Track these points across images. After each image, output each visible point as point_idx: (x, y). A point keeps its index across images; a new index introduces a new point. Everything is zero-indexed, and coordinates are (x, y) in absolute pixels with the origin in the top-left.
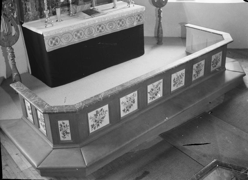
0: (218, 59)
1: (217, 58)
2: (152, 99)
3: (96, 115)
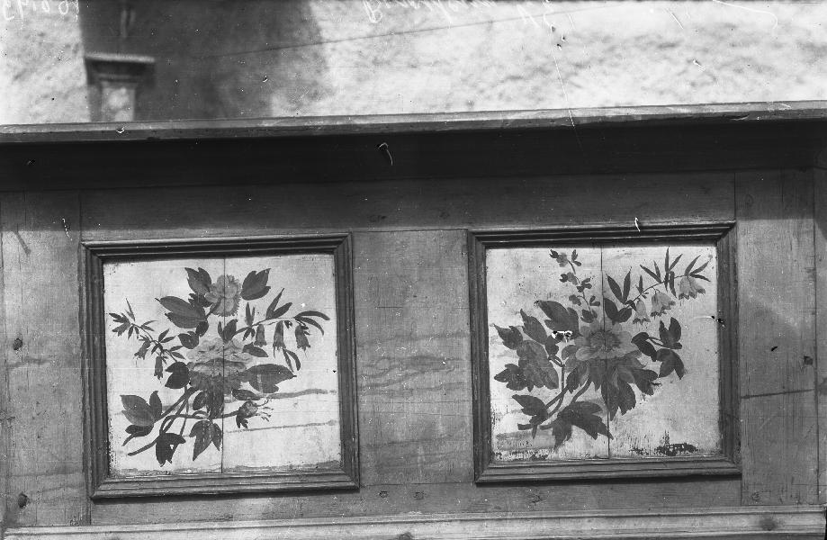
0: (630, 328)
1: (617, 316)
2: (562, 434)
3: (190, 314)
